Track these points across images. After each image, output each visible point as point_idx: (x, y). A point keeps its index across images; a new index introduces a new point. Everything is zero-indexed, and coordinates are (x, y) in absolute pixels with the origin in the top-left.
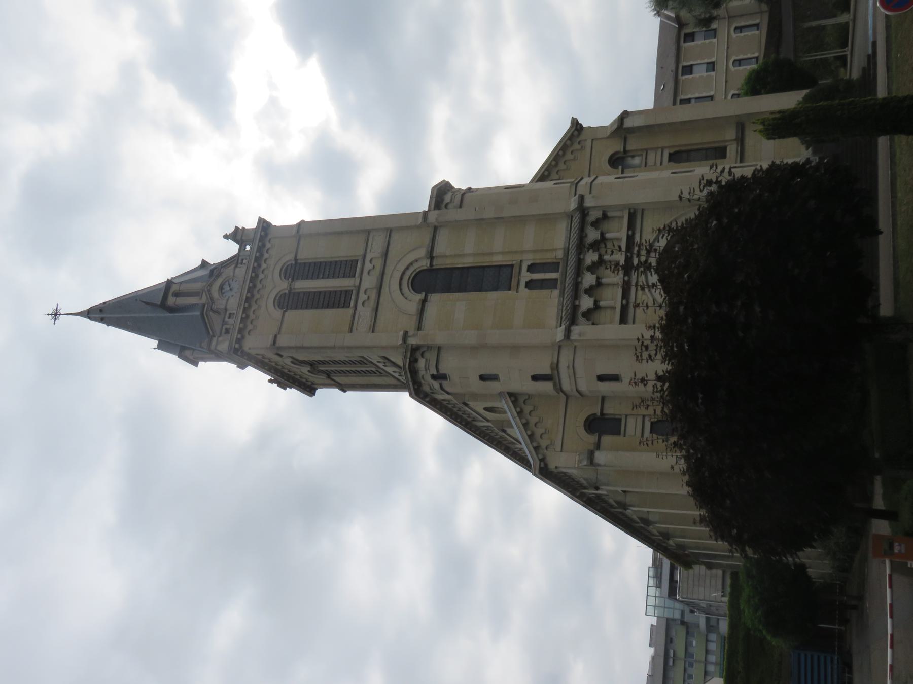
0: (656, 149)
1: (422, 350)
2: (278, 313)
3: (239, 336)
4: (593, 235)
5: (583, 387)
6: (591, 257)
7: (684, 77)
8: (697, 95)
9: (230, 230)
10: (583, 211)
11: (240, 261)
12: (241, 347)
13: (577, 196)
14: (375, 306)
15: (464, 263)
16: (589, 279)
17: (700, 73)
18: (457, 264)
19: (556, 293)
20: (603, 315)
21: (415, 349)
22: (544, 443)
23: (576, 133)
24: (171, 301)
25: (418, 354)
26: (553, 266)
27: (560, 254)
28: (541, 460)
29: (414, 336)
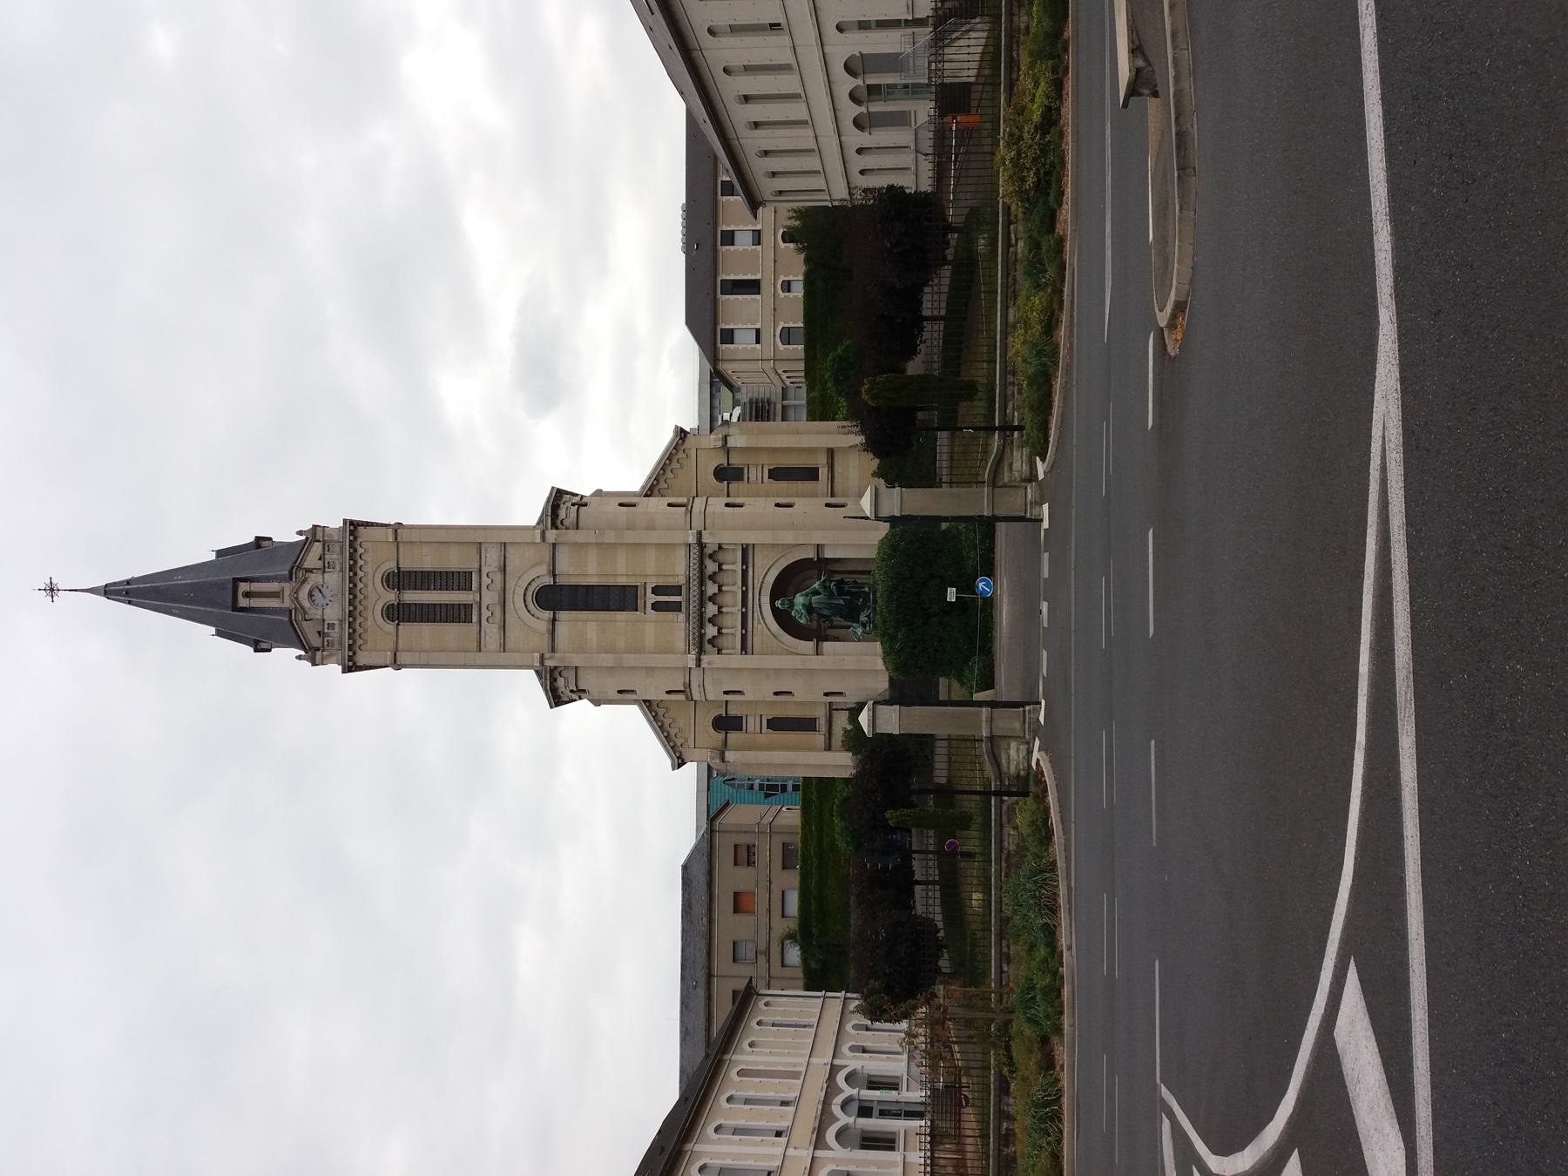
2: (390, 627)
3: (351, 653)
7: (725, 198)
11: (326, 565)
12: (354, 663)
14: (502, 623)
17: (743, 242)
19: (682, 616)
21: (553, 670)
22: (679, 742)
26: (676, 590)
28: (678, 758)
29: (550, 658)
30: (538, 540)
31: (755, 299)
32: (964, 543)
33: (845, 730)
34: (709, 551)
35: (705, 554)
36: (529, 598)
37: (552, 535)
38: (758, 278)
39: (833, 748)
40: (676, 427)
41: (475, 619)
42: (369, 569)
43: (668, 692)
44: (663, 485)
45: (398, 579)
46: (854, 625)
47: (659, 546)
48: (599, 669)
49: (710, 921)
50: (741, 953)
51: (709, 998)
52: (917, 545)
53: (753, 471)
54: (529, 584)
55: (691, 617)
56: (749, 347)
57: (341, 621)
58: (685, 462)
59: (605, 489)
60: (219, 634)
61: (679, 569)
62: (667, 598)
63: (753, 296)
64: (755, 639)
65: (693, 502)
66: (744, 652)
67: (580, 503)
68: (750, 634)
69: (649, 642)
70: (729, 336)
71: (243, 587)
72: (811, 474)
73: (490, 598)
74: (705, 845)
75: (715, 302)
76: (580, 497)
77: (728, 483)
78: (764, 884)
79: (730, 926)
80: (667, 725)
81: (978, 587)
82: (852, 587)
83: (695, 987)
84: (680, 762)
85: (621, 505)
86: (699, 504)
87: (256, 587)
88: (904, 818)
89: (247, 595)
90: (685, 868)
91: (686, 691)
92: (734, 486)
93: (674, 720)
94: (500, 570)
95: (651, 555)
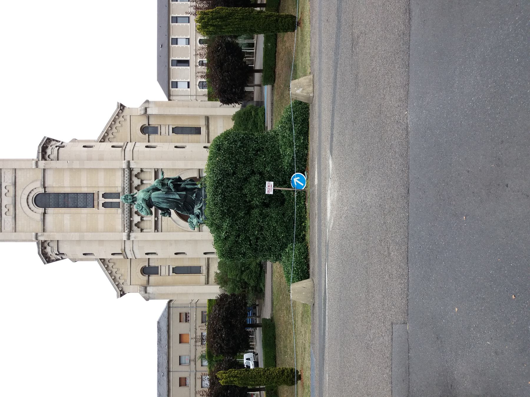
0: (165, 125)
1: (48, 242)
13: (126, 161)
14: (14, 216)
15: (65, 191)
17: (182, 43)
18: (61, 191)
19: (120, 210)
21: (43, 243)
22: (121, 282)
23: (121, 111)
26: (117, 195)
28: (121, 291)
29: (41, 235)
31: (187, 68)
32: (281, 142)
33: (217, 273)
37: (42, 164)
38: (189, 59)
39: (210, 283)
40: (118, 103)
43: (113, 254)
44: (110, 136)
46: (190, 216)
47: (105, 169)
48: (72, 241)
49: (169, 347)
50: (183, 361)
51: (169, 381)
52: (239, 144)
53: (163, 128)
54: (30, 192)
55: (125, 211)
56: (185, 90)
58: (123, 123)
59: (78, 139)
63: (186, 67)
64: (163, 223)
65: (126, 145)
66: (156, 231)
67: (61, 146)
69: (101, 226)
70: (175, 85)
72: (197, 131)
74: (166, 314)
75: (169, 69)
76: (61, 142)
77: (149, 135)
78: (193, 330)
79: (177, 349)
80: (114, 273)
81: (293, 182)
82: (187, 184)
83: (163, 376)
84: (122, 293)
85: (84, 147)
86: (130, 146)
88: (232, 379)
90: (158, 323)
91: (123, 253)
92: (152, 137)
93: (118, 269)
94: (12, 185)
95: (101, 174)
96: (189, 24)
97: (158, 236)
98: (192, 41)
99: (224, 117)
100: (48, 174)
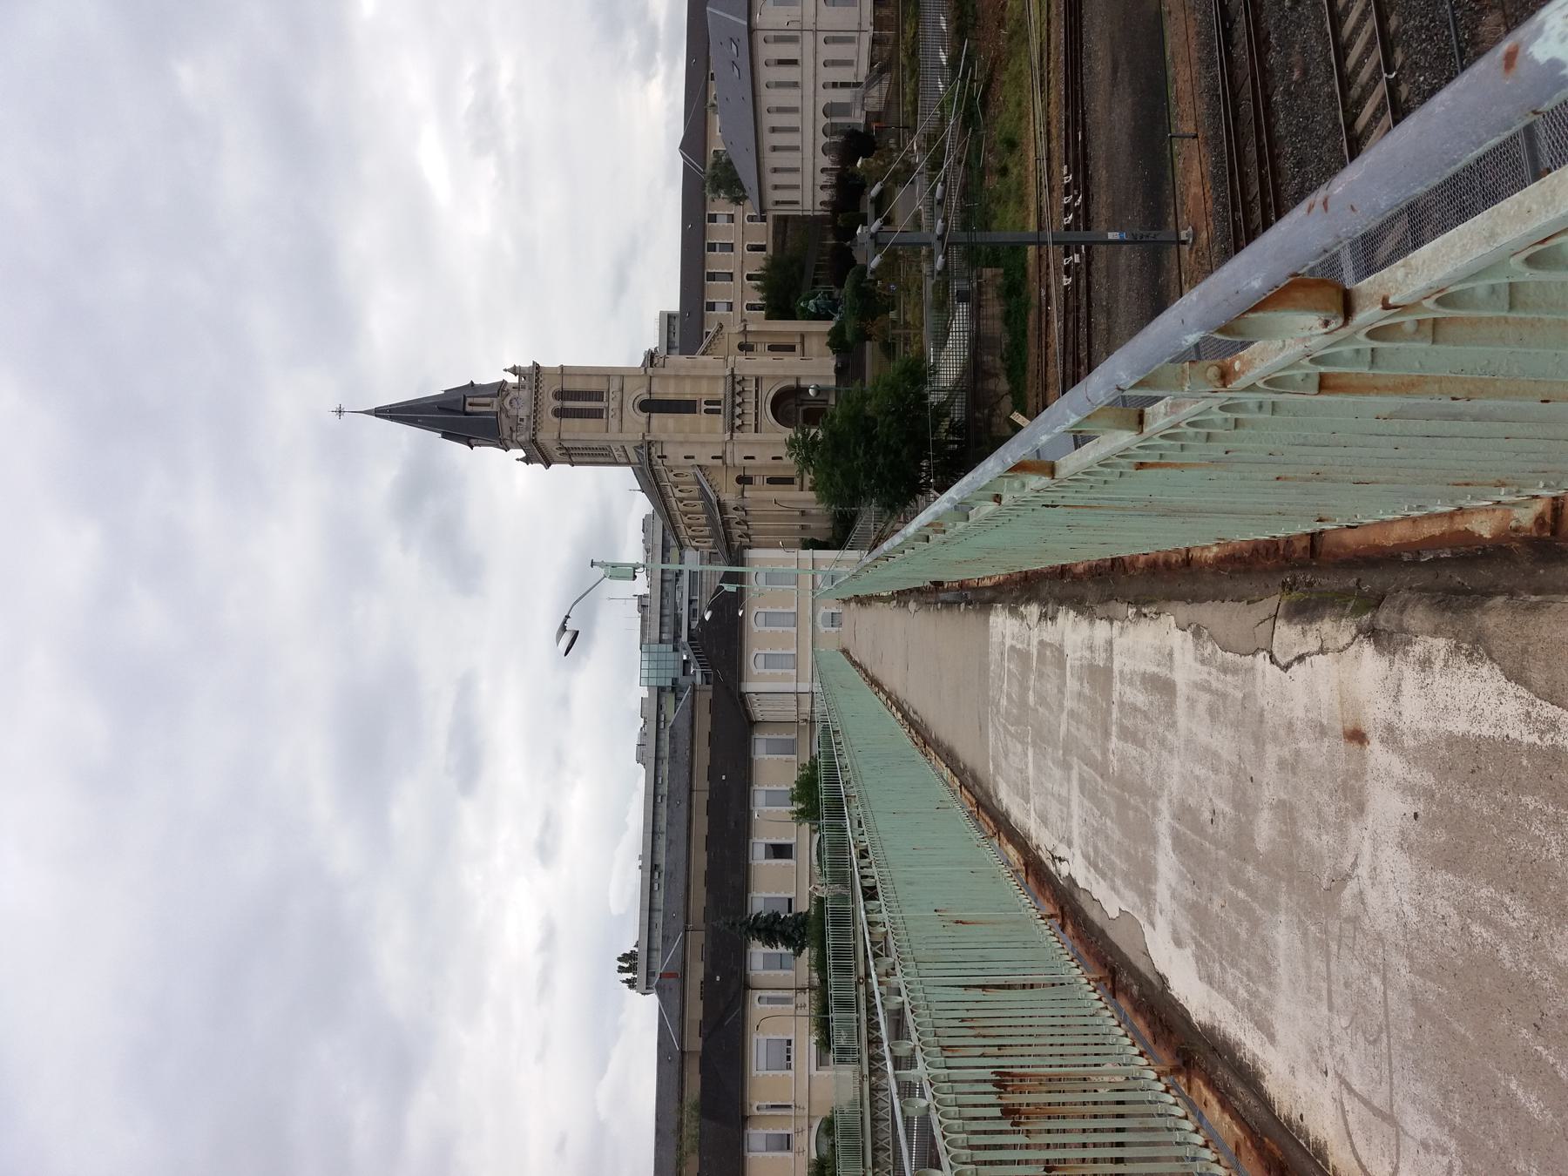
2: (556, 420)
4: (738, 388)
5: (736, 462)
6: (739, 400)
8: (721, 242)
9: (509, 366)
10: (733, 376)
16: (738, 411)
19: (721, 416)
20: (746, 428)
21: (649, 442)
24: (469, 409)
25: (651, 445)
26: (718, 403)
27: (722, 397)
30: (643, 373)
34: (737, 380)
35: (735, 380)
36: (636, 406)
37: (650, 370)
41: (604, 416)
42: (545, 389)
45: (561, 395)
48: (676, 442)
49: (692, 752)
57: (528, 417)
60: (445, 435)
61: (720, 390)
62: (713, 407)
68: (759, 425)
71: (469, 400)
72: (792, 348)
73: (614, 405)
87: (476, 400)
89: (470, 404)
96: (732, 283)
97: (758, 436)
98: (737, 307)
99: (818, 334)
100: (655, 381)
